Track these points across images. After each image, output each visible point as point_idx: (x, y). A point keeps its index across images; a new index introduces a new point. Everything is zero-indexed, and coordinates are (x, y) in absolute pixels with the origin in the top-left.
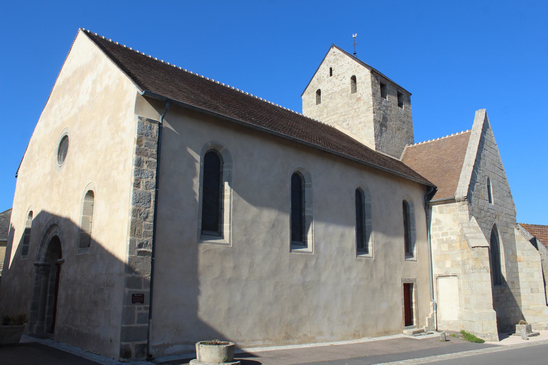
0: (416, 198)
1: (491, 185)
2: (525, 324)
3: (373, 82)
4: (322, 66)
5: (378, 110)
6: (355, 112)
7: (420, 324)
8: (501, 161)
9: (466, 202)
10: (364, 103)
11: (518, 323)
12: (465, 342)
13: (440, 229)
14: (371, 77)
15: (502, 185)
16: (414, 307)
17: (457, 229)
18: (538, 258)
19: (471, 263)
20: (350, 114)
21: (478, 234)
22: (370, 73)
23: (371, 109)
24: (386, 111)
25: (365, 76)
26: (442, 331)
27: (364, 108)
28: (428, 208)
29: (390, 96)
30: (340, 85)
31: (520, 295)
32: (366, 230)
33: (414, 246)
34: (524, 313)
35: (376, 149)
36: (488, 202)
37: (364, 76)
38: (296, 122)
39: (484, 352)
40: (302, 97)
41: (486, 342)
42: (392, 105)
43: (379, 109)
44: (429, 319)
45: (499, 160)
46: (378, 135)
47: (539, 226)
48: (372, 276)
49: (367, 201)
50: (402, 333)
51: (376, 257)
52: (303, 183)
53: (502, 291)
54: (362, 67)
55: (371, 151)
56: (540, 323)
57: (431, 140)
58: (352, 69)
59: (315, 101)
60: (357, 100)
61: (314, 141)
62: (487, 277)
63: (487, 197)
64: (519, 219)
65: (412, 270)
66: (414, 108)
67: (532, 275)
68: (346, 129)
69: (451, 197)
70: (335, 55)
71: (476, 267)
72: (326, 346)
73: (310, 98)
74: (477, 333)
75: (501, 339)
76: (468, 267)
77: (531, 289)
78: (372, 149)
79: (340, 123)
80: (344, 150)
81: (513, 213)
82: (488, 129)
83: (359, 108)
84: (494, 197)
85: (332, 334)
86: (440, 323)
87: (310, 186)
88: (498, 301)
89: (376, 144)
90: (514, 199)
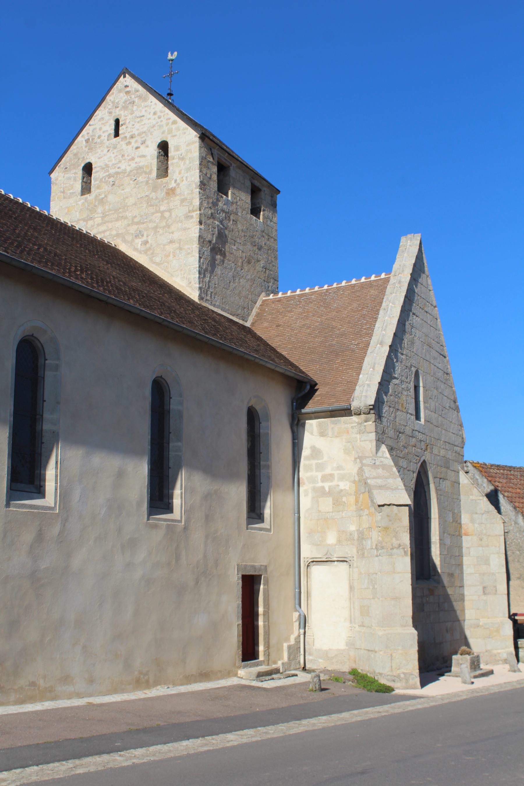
0: (275, 404)
1: (421, 384)
2: (469, 653)
4: (99, 113)
5: (209, 218)
6: (163, 217)
7: (273, 657)
8: (442, 338)
9: (372, 416)
10: (183, 201)
11: (456, 653)
12: (358, 691)
13: (320, 467)
14: (200, 147)
15: (443, 386)
16: (261, 623)
17: (352, 469)
18: (499, 529)
19: (375, 536)
20: (151, 221)
21: (390, 481)
22: (197, 139)
23: (196, 215)
24: (225, 222)
25: (188, 145)
26: (313, 671)
27: (181, 211)
28: (297, 425)
29: (236, 192)
30: (133, 159)
31: (463, 600)
32: (171, 465)
33: (265, 501)
34: (468, 633)
35: (201, 298)
36: (413, 417)
37: (186, 142)
38: (35, 229)
39: (392, 711)
40: (53, 176)
41: (397, 692)
42: (240, 210)
43: (212, 216)
44: (289, 647)
45: (438, 337)
46: (206, 270)
47: (504, 468)
48: (178, 558)
49: (174, 406)
50: (236, 675)
51: (188, 520)
52: (41, 361)
53: (432, 592)
54: (182, 124)
55: (188, 301)
56: (495, 652)
57: (312, 287)
59: (78, 186)
60: (168, 194)
61: (70, 272)
62: (404, 565)
63: (412, 410)
64: (471, 454)
65: (261, 547)
66: (284, 219)
67: (487, 562)
68: (140, 252)
69: (344, 405)
70: (128, 93)
71: (384, 544)
72: (78, 707)
73: (69, 178)
74: (381, 674)
75: (424, 683)
76: (368, 544)
77: (484, 588)
78: (192, 297)
79: (129, 238)
80: (133, 298)
81: (458, 441)
82: (423, 276)
83: (170, 211)
84: (426, 408)
85: (91, 681)
86: (310, 654)
87: (56, 368)
88: (423, 611)
89: (200, 288)
90: (463, 413)
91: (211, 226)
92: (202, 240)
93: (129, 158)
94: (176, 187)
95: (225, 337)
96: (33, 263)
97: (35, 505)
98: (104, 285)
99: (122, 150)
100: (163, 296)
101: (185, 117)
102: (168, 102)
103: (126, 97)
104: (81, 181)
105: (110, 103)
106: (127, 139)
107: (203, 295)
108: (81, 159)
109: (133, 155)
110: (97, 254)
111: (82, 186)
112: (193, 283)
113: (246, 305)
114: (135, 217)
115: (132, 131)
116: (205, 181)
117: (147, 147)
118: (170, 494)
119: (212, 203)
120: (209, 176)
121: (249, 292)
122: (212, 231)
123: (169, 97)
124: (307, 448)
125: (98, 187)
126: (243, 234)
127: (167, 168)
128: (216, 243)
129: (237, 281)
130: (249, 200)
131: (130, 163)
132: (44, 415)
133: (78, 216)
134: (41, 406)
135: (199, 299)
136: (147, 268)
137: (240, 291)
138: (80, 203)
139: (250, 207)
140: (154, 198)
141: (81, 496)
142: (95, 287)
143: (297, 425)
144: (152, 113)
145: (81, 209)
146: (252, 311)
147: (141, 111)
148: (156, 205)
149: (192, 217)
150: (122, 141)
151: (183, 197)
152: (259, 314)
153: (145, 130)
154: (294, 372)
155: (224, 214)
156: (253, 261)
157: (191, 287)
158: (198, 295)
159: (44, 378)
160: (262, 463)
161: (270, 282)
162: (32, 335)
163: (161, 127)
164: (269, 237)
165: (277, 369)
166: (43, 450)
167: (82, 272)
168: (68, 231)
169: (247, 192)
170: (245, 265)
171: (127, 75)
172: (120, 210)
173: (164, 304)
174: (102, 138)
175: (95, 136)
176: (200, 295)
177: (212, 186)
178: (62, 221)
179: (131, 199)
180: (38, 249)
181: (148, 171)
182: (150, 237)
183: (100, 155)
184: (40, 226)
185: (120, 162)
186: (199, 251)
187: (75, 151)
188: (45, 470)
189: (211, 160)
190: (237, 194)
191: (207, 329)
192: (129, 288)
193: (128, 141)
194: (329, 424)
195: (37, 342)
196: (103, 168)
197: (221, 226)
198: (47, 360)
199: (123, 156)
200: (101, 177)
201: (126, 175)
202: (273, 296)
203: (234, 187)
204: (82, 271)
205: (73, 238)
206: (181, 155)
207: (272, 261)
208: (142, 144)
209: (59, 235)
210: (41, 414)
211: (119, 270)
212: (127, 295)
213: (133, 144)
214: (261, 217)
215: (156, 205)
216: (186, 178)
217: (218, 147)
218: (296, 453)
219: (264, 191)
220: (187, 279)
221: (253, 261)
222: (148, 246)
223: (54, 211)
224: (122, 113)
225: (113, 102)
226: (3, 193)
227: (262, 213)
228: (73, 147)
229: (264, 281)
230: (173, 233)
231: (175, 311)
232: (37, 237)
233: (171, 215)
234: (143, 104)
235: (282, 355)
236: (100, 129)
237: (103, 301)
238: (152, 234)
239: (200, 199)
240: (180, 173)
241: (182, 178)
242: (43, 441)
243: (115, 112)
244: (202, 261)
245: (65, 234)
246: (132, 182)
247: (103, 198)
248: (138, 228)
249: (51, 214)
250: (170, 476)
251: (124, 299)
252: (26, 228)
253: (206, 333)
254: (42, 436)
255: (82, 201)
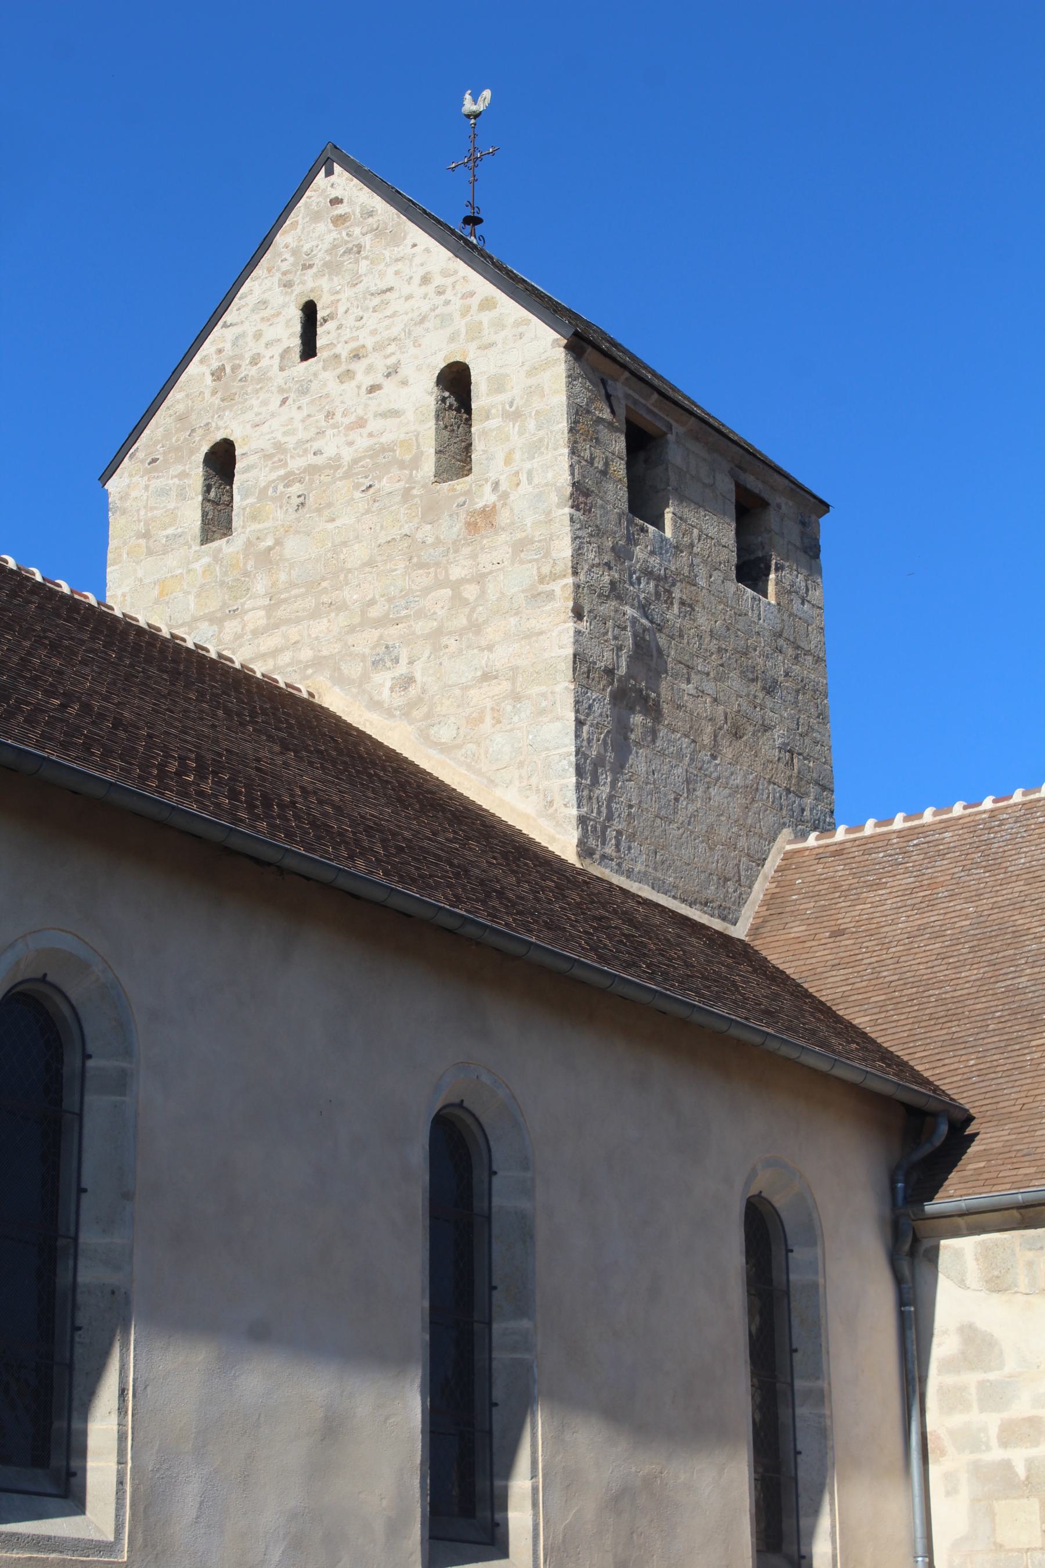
0: (839, 1186)
3: (578, 415)
5: (604, 597)
6: (458, 600)
10: (519, 547)
13: (993, 1396)
14: (571, 378)
20: (420, 614)
22: (560, 353)
23: (563, 588)
24: (656, 609)
28: (910, 1256)
29: (690, 514)
30: (361, 423)
32: (498, 1394)
33: (815, 1512)
35: (585, 851)
37: (526, 366)
38: (54, 648)
40: (113, 486)
42: (702, 571)
43: (615, 592)
46: (599, 762)
49: (503, 1198)
52: (72, 1061)
54: (511, 309)
58: (445, 320)
59: (191, 515)
60: (472, 527)
61: (163, 775)
66: (849, 591)
68: (389, 713)
70: (339, 220)
73: (164, 492)
78: (555, 848)
79: (353, 670)
83: (480, 579)
87: (121, 1082)
89: (582, 820)
91: (610, 623)
92: (584, 669)
93: (347, 421)
94: (499, 505)
95: (665, 974)
96: (43, 749)
97: (49, 1538)
98: (282, 817)
99: (327, 395)
100: (463, 846)
101: (520, 286)
102: (468, 243)
103: (334, 235)
104: (200, 498)
105: (287, 256)
106: (340, 363)
107: (592, 842)
108: (200, 432)
109: (360, 412)
110: (253, 722)
111: (205, 514)
112: (558, 803)
113: (730, 872)
114: (372, 602)
115: (357, 338)
116: (589, 482)
117: (404, 383)
118: (496, 1492)
119: (613, 549)
120: (600, 466)
121: (741, 826)
122: (615, 638)
123: (469, 228)
124: (945, 1332)
125: (255, 517)
126: (713, 646)
127: (468, 448)
128: (629, 675)
129: (699, 793)
130: (729, 536)
131: (353, 435)
132: (83, 1238)
133: (192, 606)
134: (73, 1207)
135: (579, 855)
136: (412, 763)
137: (711, 826)
138: (198, 566)
139: (734, 560)
140: (430, 540)
141: (201, 1503)
142: (242, 821)
143: (912, 1253)
144: (417, 280)
145: (202, 586)
146: (750, 887)
147: (382, 275)
148: (437, 564)
149: (550, 596)
150: (324, 369)
151: (519, 535)
152: (773, 896)
153: (395, 331)
154: (895, 1079)
155: (652, 584)
156: (751, 729)
157: (552, 817)
158: (575, 841)
159: (80, 1116)
160: (799, 1384)
161: (807, 794)
162: (43, 979)
163: (445, 320)
164: (800, 652)
165: (839, 1072)
166: (79, 1350)
167: (201, 776)
168: (162, 651)
169: (724, 514)
170: (725, 742)
171: (337, 168)
172: (324, 584)
173: (466, 871)
174: (264, 363)
175: (241, 357)
176: (581, 843)
177: (610, 496)
178: (142, 624)
179: (356, 547)
180: (63, 706)
181: (408, 457)
182: (418, 666)
183: (258, 414)
184: (72, 639)
185: (321, 433)
186: (577, 702)
187: (181, 408)
188: (85, 1420)
189: (606, 415)
190: (693, 520)
191: (605, 947)
192: (354, 823)
193: (343, 368)
194: (1018, 1249)
195: (58, 999)
196: (268, 457)
197: (644, 621)
198: (90, 1057)
199: (330, 415)
200: (263, 484)
201: (340, 473)
202: (817, 839)
203: (682, 499)
204: (201, 773)
205: (175, 674)
206: (511, 405)
207: (811, 728)
208: (388, 375)
209: (132, 666)
210: (72, 1233)
211: (323, 768)
212: (347, 843)
213: (359, 377)
214: (771, 588)
215: (437, 564)
216: (530, 474)
217: (627, 374)
218: (913, 1348)
219: (779, 506)
220: (538, 791)
221: (751, 729)
222: (413, 691)
223: (119, 593)
224: (324, 283)
225: (295, 252)
226: (12, 564)
227: (772, 576)
228: (175, 395)
229: (788, 791)
230: (490, 648)
231: (501, 894)
232: (60, 673)
233: (483, 592)
234: (387, 253)
235: (854, 1027)
236: (258, 335)
237: (269, 864)
238: (427, 653)
239: (575, 538)
240: (508, 461)
241: (517, 473)
242: (78, 1323)
243: (303, 283)
244: (585, 735)
245: (149, 660)
246: (358, 495)
247: (270, 549)
248: (381, 637)
249: (109, 602)
250: (496, 1433)
251: (337, 858)
252: (27, 644)
253: (602, 959)
254: (75, 1306)
255: (206, 560)
